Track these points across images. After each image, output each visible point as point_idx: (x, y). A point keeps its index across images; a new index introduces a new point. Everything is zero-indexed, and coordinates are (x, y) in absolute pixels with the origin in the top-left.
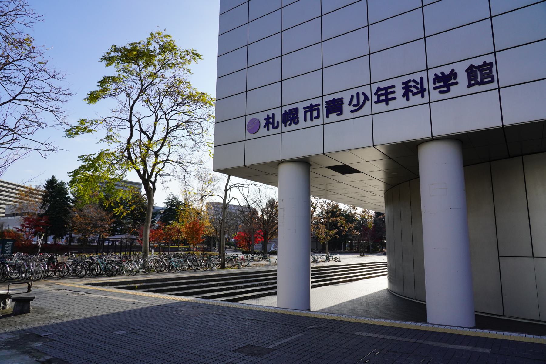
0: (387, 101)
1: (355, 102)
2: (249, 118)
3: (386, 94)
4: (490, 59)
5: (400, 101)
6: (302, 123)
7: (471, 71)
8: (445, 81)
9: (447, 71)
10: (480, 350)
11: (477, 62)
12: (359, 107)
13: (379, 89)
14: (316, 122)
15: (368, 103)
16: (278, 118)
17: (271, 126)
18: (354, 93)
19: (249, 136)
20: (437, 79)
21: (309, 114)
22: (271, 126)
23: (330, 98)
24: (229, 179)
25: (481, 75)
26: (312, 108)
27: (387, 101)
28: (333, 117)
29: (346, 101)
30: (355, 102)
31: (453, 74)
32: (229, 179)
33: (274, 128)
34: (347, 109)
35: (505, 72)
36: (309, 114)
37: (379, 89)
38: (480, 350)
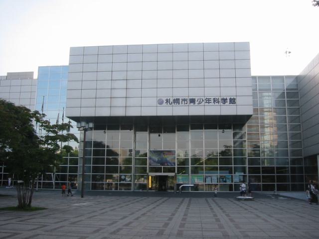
0: (209, 103)
1: (199, 101)
2: (158, 98)
3: (209, 100)
4: (235, 97)
5: (212, 104)
6: (212, 98)
7: (231, 99)
8: (224, 101)
9: (225, 98)
10: (176, 139)
11: (232, 98)
12: (200, 103)
13: (207, 99)
14: (187, 105)
15: (203, 102)
16: (171, 101)
17: (168, 103)
18: (199, 98)
19: (158, 105)
20: (222, 99)
21: (183, 102)
22: (168, 103)
23: (191, 98)
24: (135, 136)
25: (233, 101)
26: (184, 100)
27: (209, 103)
28: (192, 104)
29: (196, 100)
30: (199, 101)
31: (226, 99)
32: (135, 136)
33: (170, 104)
34: (197, 103)
35: (238, 101)
36: (183, 102)
37: (207, 99)
38: (176, 139)
